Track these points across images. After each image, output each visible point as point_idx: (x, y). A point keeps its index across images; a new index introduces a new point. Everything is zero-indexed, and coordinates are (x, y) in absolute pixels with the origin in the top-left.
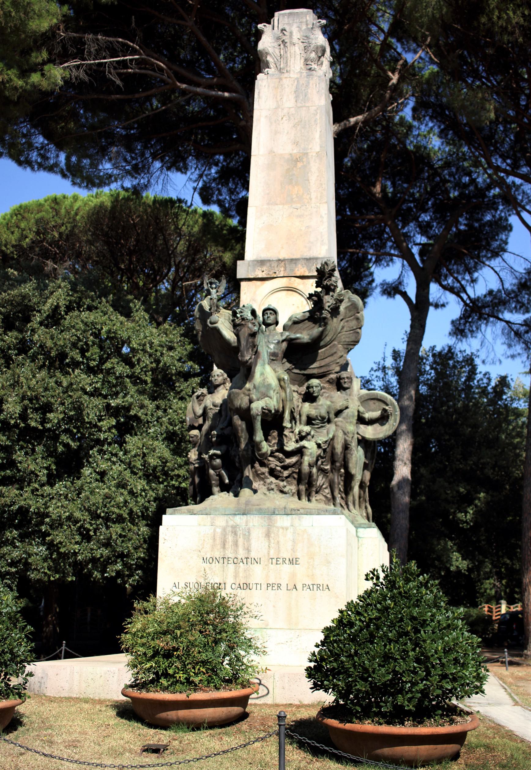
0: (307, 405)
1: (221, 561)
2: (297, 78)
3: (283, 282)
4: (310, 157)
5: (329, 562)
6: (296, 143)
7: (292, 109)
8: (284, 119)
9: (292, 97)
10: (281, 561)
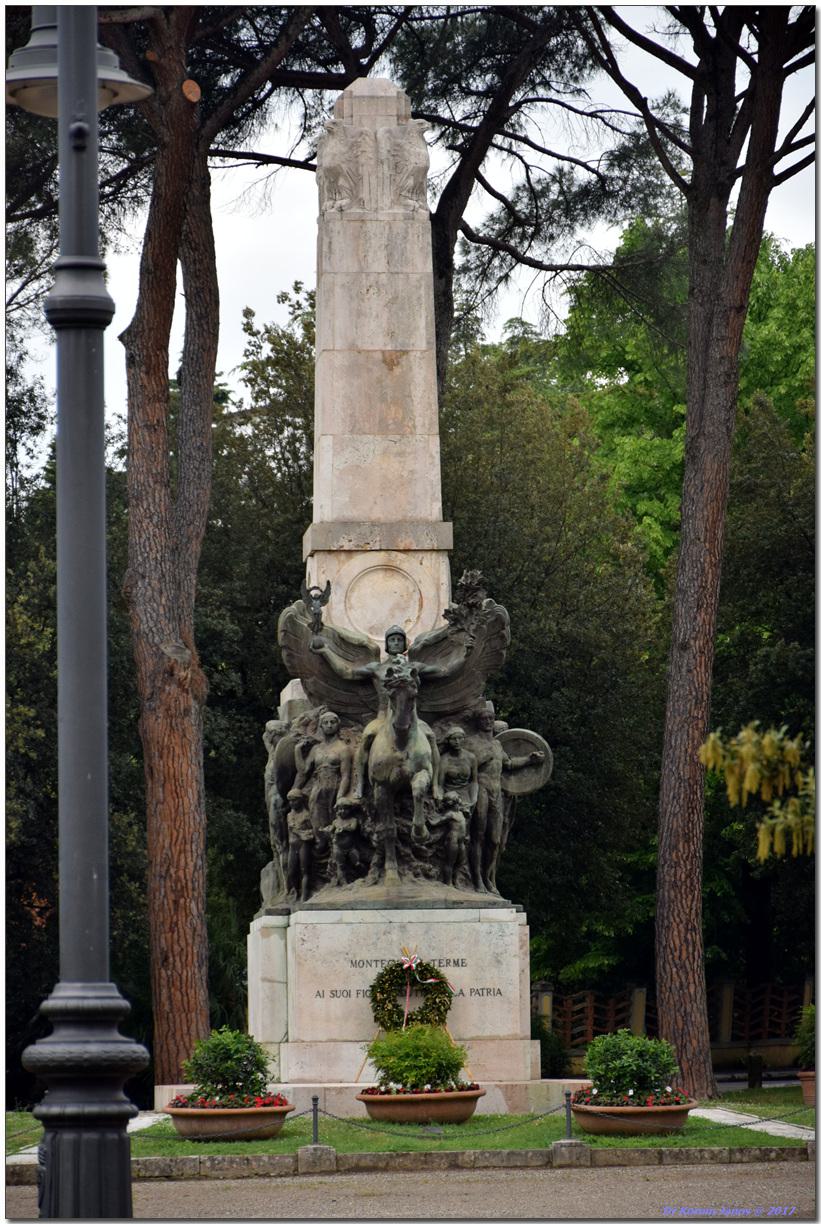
0: (447, 758)
1: (374, 964)
2: (389, 223)
3: (379, 558)
4: (412, 358)
5: (499, 962)
6: (391, 334)
7: (383, 276)
8: (371, 291)
9: (382, 255)
10: (444, 963)
